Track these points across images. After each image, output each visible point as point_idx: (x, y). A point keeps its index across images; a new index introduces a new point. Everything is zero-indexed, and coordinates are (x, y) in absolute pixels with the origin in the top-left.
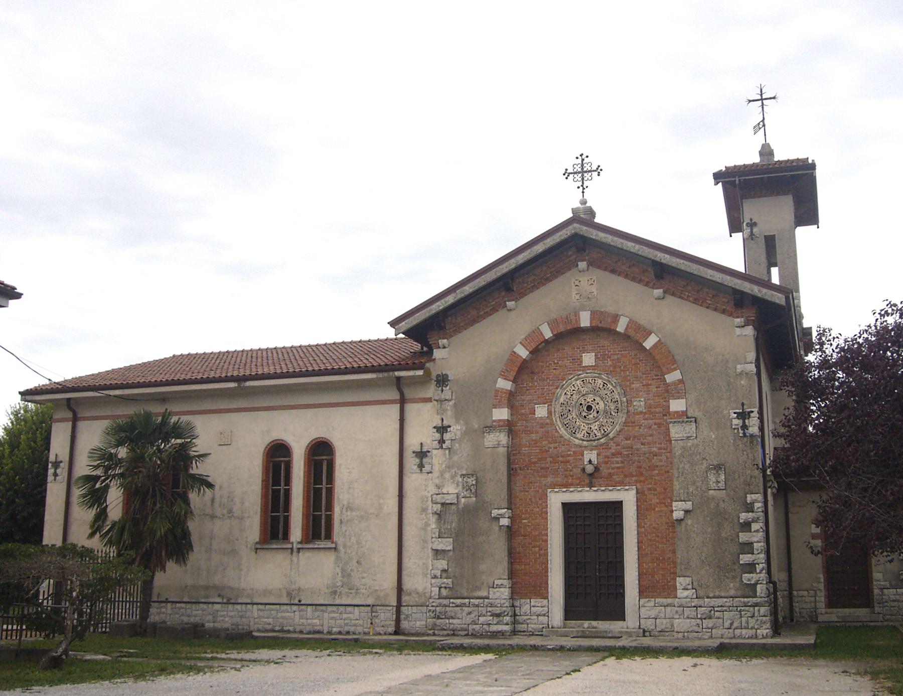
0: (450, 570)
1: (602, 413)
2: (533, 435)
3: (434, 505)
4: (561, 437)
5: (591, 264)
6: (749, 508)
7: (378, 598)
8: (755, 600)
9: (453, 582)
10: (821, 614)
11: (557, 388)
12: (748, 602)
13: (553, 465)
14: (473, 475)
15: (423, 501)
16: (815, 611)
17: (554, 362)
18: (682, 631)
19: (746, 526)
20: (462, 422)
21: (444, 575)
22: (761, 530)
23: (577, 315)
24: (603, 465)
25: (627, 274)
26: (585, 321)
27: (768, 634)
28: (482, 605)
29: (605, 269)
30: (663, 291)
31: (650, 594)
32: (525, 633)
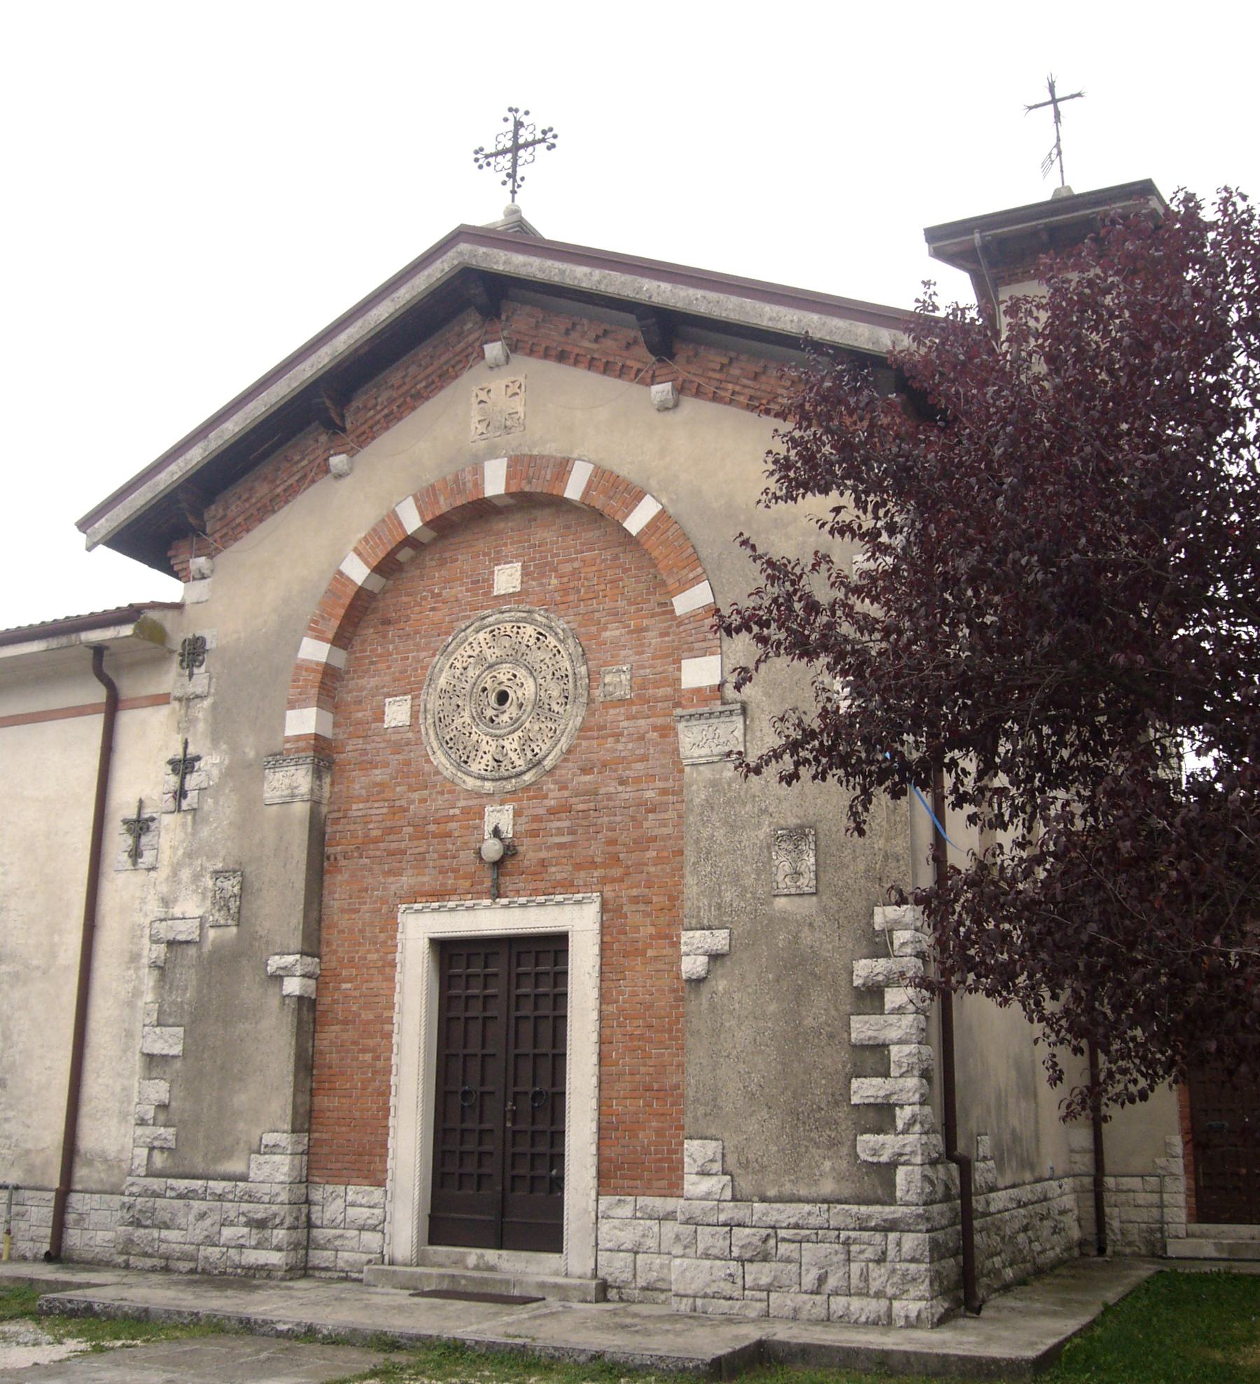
0: (174, 1104)
1: (529, 709)
2: (377, 772)
3: (154, 946)
4: (438, 773)
5: (514, 347)
6: (879, 945)
7: (30, 1170)
8: (888, 1212)
9: (177, 1136)
10: (1177, 1237)
11: (434, 655)
12: (869, 1216)
13: (415, 843)
14: (235, 872)
15: (133, 937)
16: (1161, 1230)
17: (432, 592)
18: (690, 1292)
19: (870, 997)
20: (224, 747)
21: (162, 1118)
22: (911, 1008)
23: (478, 471)
24: (527, 841)
25: (593, 359)
26: (495, 483)
27: (924, 1315)
28: (231, 1197)
29: (546, 355)
30: (673, 387)
31: (626, 1183)
32: (329, 1274)
